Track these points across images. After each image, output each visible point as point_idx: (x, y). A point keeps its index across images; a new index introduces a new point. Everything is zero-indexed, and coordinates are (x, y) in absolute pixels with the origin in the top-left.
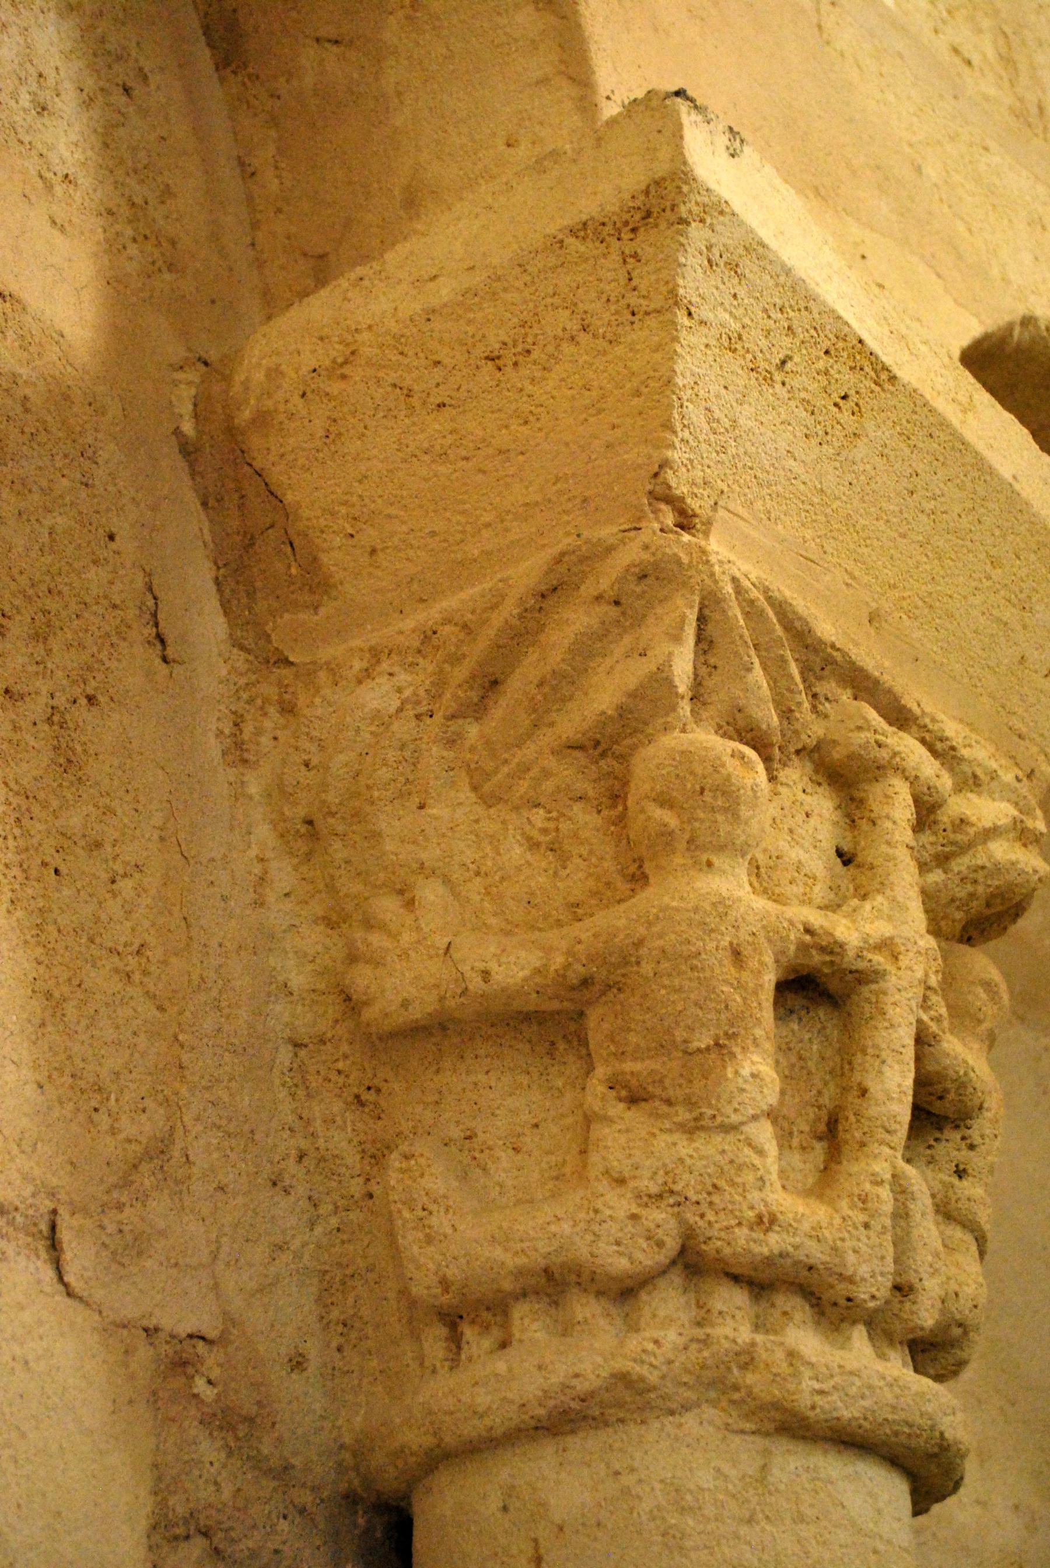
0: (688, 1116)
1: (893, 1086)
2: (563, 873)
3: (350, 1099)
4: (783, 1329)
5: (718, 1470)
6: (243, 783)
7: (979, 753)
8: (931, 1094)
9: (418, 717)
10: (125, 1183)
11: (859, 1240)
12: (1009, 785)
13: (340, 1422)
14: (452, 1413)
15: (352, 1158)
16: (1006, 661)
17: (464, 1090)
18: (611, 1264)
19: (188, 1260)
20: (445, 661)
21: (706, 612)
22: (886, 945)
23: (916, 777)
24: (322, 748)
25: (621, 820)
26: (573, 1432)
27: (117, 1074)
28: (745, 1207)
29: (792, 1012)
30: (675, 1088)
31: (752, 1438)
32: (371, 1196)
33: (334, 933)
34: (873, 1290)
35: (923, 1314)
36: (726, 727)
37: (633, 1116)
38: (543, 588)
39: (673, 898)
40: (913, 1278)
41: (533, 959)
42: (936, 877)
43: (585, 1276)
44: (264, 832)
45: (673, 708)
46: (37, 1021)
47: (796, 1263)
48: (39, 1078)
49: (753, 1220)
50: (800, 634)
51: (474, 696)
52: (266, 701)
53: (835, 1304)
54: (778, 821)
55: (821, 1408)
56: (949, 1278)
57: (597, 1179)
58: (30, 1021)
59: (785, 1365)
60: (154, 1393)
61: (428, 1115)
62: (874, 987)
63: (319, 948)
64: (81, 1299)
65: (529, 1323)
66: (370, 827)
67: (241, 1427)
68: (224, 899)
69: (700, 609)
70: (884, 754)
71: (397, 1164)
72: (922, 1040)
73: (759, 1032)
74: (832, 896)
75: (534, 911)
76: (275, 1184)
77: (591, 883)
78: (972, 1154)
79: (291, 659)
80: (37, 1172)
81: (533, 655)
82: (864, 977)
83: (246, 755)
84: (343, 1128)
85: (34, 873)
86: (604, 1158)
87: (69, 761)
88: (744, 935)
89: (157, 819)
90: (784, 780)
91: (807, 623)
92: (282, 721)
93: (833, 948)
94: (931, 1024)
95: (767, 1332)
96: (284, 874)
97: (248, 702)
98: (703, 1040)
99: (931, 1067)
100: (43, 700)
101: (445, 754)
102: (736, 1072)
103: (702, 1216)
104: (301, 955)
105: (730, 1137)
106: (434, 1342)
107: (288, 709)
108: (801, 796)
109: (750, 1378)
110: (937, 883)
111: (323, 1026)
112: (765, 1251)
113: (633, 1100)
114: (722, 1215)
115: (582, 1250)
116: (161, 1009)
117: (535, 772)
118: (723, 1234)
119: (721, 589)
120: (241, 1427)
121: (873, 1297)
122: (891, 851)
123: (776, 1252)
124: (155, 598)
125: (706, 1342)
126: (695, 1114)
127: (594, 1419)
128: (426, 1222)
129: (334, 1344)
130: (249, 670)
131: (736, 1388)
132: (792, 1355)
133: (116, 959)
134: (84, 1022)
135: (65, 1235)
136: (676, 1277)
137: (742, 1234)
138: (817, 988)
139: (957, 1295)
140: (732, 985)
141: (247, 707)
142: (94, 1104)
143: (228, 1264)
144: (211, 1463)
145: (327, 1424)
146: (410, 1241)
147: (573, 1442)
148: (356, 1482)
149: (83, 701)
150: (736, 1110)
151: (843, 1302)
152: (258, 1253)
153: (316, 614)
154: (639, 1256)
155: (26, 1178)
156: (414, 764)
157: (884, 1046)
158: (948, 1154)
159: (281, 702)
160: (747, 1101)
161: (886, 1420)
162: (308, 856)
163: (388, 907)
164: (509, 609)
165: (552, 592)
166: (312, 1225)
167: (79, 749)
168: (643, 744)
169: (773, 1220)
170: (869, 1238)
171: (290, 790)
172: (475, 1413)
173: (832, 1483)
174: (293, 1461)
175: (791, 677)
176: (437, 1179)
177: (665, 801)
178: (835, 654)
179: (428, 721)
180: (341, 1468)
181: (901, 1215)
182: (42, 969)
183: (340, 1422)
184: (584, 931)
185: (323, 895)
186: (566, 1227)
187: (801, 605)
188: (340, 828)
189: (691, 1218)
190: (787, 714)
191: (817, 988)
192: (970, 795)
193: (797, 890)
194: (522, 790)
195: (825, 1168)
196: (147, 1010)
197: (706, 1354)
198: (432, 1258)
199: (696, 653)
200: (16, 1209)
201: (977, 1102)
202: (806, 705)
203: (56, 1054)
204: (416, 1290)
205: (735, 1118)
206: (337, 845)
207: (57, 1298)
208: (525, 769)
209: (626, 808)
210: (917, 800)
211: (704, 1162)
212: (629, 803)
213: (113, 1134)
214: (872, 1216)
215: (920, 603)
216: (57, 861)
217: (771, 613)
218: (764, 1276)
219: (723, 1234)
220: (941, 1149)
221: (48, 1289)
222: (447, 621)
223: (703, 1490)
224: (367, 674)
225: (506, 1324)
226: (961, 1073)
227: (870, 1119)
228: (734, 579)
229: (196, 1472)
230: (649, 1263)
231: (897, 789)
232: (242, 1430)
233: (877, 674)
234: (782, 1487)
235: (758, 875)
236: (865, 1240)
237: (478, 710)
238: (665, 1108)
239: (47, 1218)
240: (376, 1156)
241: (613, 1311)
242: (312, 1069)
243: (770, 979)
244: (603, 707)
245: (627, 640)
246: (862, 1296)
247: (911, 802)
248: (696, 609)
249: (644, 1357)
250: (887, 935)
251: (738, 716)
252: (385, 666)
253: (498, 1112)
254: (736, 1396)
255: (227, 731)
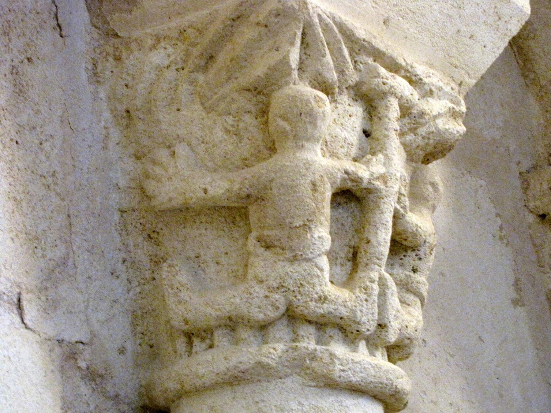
0: (290, 255)
1: (383, 238)
2: (239, 145)
3: (145, 236)
4: (329, 343)
5: (299, 402)
6: (97, 92)
7: (434, 79)
8: (401, 238)
9: (177, 70)
10: (49, 278)
11: (362, 306)
12: (448, 92)
13: (140, 376)
14: (188, 376)
15: (146, 260)
16: (450, 33)
17: (195, 237)
18: (257, 316)
19: (76, 310)
20: (189, 45)
21: (306, 30)
22: (383, 178)
23: (402, 96)
24: (134, 79)
25: (266, 123)
26: (239, 384)
27: (45, 231)
28: (314, 293)
29: (339, 204)
30: (286, 243)
31: (314, 388)
32: (154, 279)
33: (138, 161)
34: (368, 327)
35: (390, 336)
36: (313, 81)
37: (267, 254)
38: (233, 16)
39: (286, 161)
40: (386, 321)
41: (226, 185)
42: (410, 137)
43: (246, 321)
44: (107, 115)
45: (290, 75)
46: (10, 211)
47: (335, 316)
48: (12, 236)
49: (317, 298)
50: (349, 36)
51: (203, 63)
52: (108, 54)
53: (352, 333)
54: (336, 120)
55: (343, 377)
56: (403, 320)
57: (251, 280)
58: (7, 211)
59: (328, 359)
60: (62, 367)
61: (179, 247)
62: (375, 195)
63: (132, 168)
64: (31, 330)
65: (221, 338)
66: (155, 117)
67: (98, 379)
68: (90, 146)
69: (303, 29)
70: (386, 88)
71: (166, 269)
72: (397, 217)
73: (322, 218)
74: (360, 152)
75: (227, 161)
76: (112, 274)
77: (252, 150)
78: (419, 262)
79: (119, 34)
80: (12, 277)
81: (229, 46)
82: (370, 191)
83: (99, 79)
84: (143, 249)
85: (8, 144)
86: (254, 271)
87: (20, 90)
88: (317, 177)
89: (59, 112)
90: (340, 101)
91: (352, 31)
92: (115, 63)
93: (357, 180)
94: (401, 209)
95: (322, 345)
96: (115, 135)
97: (99, 54)
98: (298, 223)
99: (400, 228)
100: (8, 64)
101: (189, 88)
102: (312, 236)
103: (295, 297)
104: (123, 170)
105: (308, 264)
106: (181, 344)
107: (118, 59)
108: (348, 108)
109: (314, 364)
110: (410, 140)
111: (134, 204)
112: (322, 311)
113: (268, 247)
114: (304, 297)
115: (244, 309)
116: (63, 200)
117: (229, 99)
118: (304, 304)
119: (312, 20)
120: (98, 379)
121: (368, 330)
122: (386, 133)
123: (326, 312)
124: (56, 6)
125: (295, 349)
126: (294, 254)
127: (248, 380)
128: (179, 294)
129: (138, 342)
130: (100, 38)
131: (308, 368)
132: (332, 356)
133: (43, 179)
134: (30, 209)
135: (24, 303)
136: (285, 321)
137: (312, 305)
138: (352, 197)
139: (407, 327)
140: (311, 199)
141: (99, 56)
142: (35, 245)
143: (92, 310)
144: (86, 395)
145: (135, 377)
146: (171, 301)
147: (239, 389)
148: (147, 401)
149: (26, 61)
150: (311, 252)
151: (355, 332)
152: (105, 305)
153: (131, 14)
154: (268, 313)
155: (8, 279)
156: (175, 91)
157: (378, 221)
158: (409, 262)
159: (115, 55)
160: (316, 248)
161: (371, 381)
162: (127, 127)
163: (162, 154)
164: (218, 26)
165: (238, 19)
166: (129, 291)
167: (24, 83)
168: (276, 90)
169: (326, 298)
170: (367, 305)
171: (119, 97)
172: (198, 376)
173: (347, 407)
174: (120, 393)
175: (344, 57)
176: (183, 277)
177: (284, 118)
178: (365, 43)
179: (182, 72)
180: (140, 395)
181: (383, 295)
182: (12, 188)
183: (140, 376)
184: (247, 173)
185: (134, 144)
186: (238, 300)
187: (350, 21)
188: (142, 116)
189: (291, 298)
190: (341, 72)
191: (352, 197)
192: (429, 99)
193: (344, 150)
194: (223, 106)
195: (351, 274)
196: (56, 200)
197: (295, 354)
198: (181, 310)
199: (301, 49)
200: (4, 293)
201: (422, 240)
202: (352, 67)
203: (19, 225)
204: (174, 323)
205: (310, 256)
206: (141, 123)
207: (22, 330)
208: (224, 97)
209: (268, 118)
210: (401, 107)
211: (297, 274)
212: (270, 117)
213: (43, 257)
214: (369, 296)
215: (409, 12)
216: (17, 138)
217: (335, 29)
218: (322, 321)
219: (304, 304)
220: (406, 260)
221: (17, 326)
222: (190, 26)
223: (292, 410)
224: (154, 47)
225: (212, 340)
226: (415, 230)
227: (370, 254)
228: (319, 16)
229: (79, 399)
230: (273, 316)
231: (391, 103)
232: (99, 380)
233: (384, 50)
234: (326, 409)
235: (326, 145)
236: (366, 306)
237: (205, 69)
238: (281, 251)
239: (16, 296)
240: (157, 262)
241: (257, 334)
242: (128, 222)
243: (328, 195)
244: (259, 73)
245: (271, 42)
246: (363, 330)
247: (398, 109)
248: (301, 30)
249: (269, 355)
250: (382, 172)
251: (319, 77)
252: (163, 44)
253: (210, 246)
254: (308, 371)
255: (90, 68)
